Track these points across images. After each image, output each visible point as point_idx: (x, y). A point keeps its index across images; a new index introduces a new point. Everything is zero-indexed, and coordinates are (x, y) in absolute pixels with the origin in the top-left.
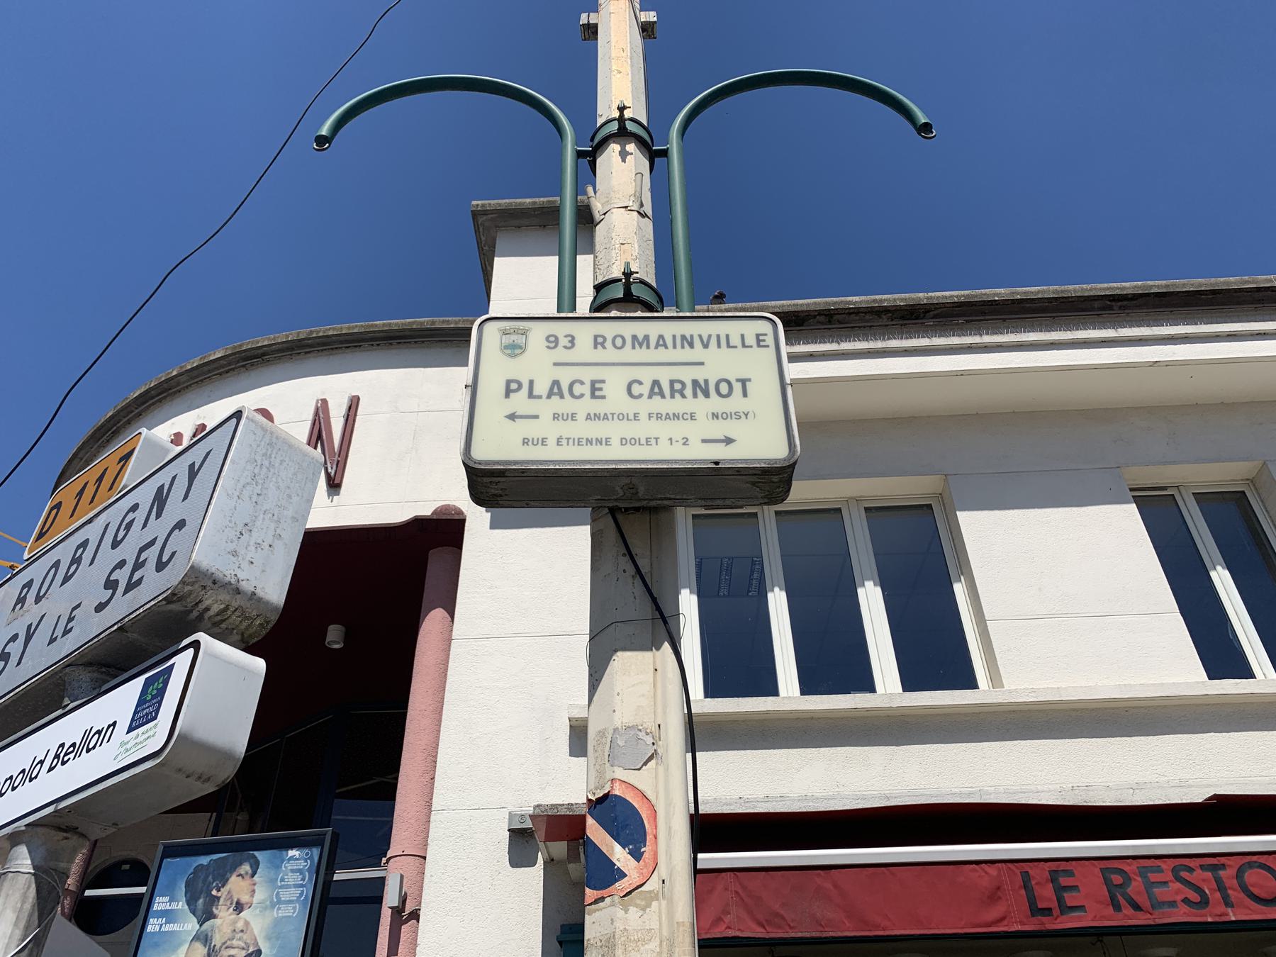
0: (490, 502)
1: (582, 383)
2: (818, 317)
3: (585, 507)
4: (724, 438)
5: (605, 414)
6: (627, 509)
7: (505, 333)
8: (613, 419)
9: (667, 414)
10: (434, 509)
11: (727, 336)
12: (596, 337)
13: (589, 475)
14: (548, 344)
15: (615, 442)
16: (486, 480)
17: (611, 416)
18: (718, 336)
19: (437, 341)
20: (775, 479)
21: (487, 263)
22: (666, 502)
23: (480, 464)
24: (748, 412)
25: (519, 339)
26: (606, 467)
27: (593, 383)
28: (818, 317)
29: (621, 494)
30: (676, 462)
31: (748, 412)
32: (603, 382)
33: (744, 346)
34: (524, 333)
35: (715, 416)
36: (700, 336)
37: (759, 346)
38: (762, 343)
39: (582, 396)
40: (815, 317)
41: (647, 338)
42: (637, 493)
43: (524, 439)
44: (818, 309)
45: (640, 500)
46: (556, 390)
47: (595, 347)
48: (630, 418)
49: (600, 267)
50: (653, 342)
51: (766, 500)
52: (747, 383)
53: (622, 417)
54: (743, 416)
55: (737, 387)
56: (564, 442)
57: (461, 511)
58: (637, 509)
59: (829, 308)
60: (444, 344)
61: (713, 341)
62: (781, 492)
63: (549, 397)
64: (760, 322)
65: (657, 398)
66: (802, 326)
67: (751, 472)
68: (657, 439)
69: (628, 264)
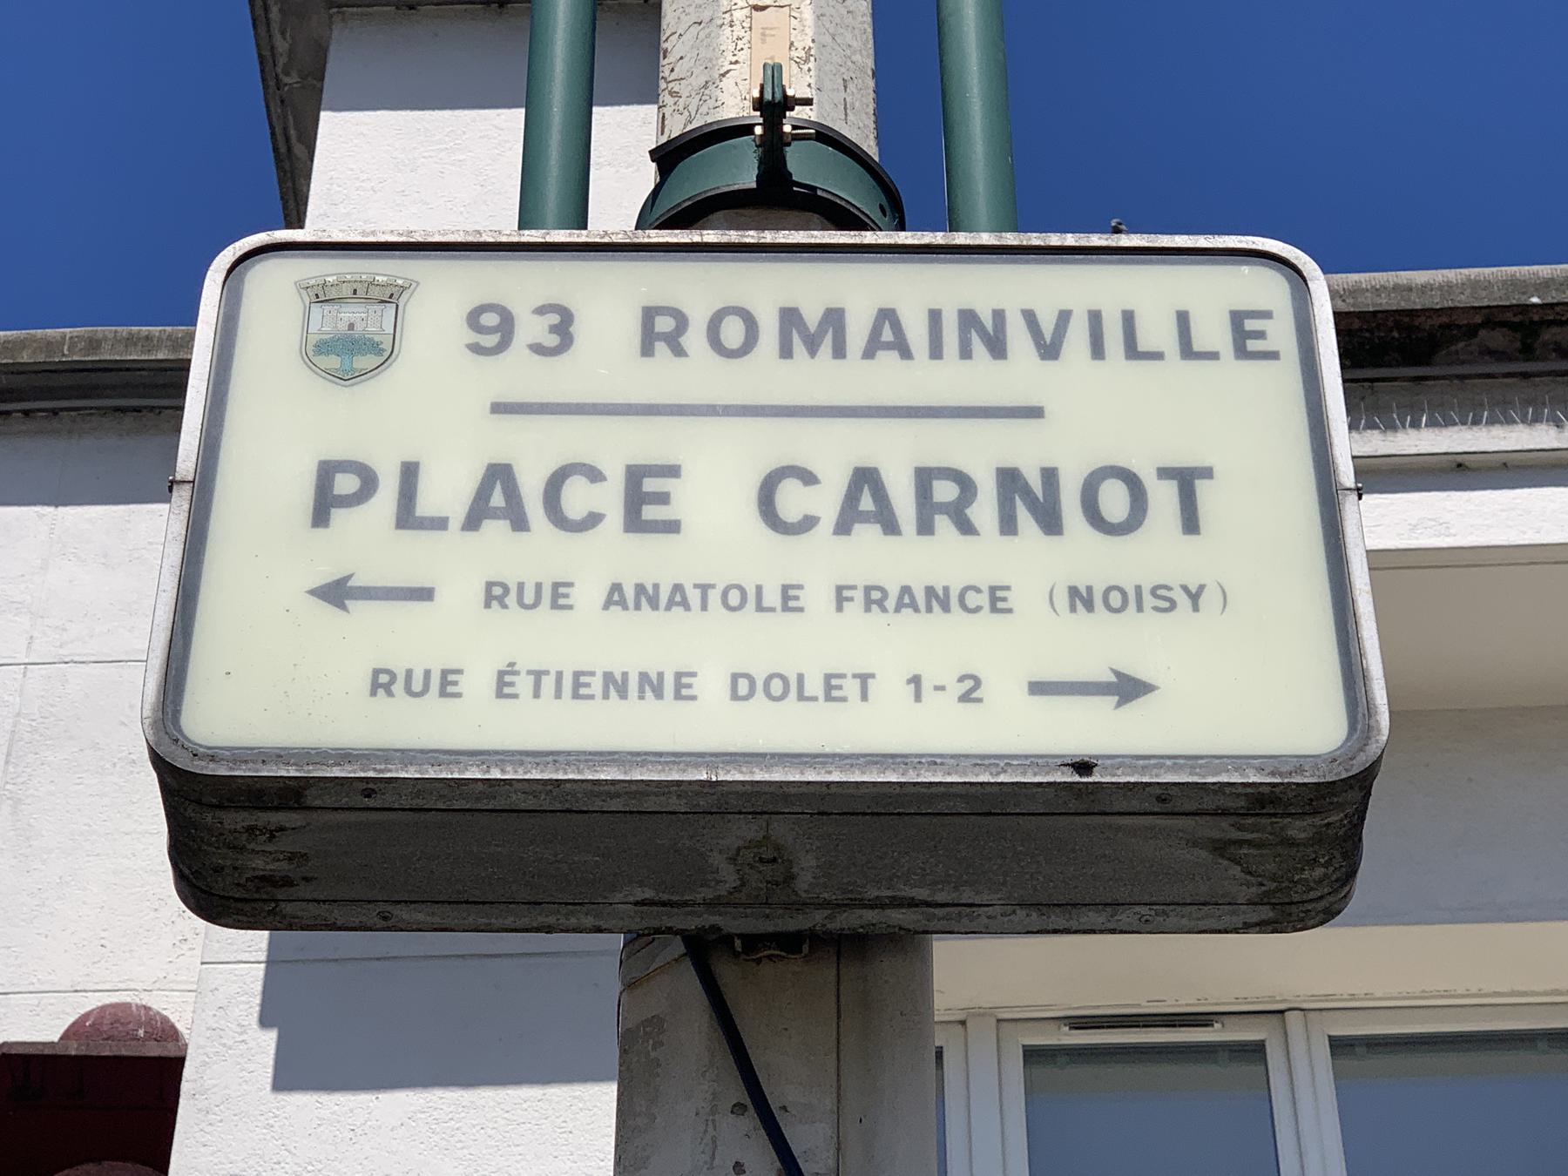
0: (247, 907)
1: (594, 475)
2: (1483, 333)
3: (599, 930)
4: (1113, 679)
5: (678, 588)
6: (753, 942)
7: (321, 296)
8: (704, 607)
9: (906, 590)
10: (71, 1020)
11: (1128, 318)
12: (649, 314)
13: (615, 805)
14: (474, 337)
15: (711, 685)
16: (236, 820)
17: (698, 592)
18: (1095, 318)
19: (104, 411)
20: (1299, 829)
21: (292, 132)
22: (898, 917)
23: (213, 758)
24: (1202, 588)
25: (371, 321)
26: (675, 777)
27: (635, 475)
28: (1483, 333)
29: (730, 877)
30: (934, 761)
31: (1202, 588)
32: (673, 471)
33: (1188, 351)
34: (392, 297)
35: (1081, 598)
36: (1030, 317)
37: (1242, 352)
38: (1252, 345)
39: (593, 520)
40: (1472, 331)
41: (834, 319)
42: (790, 878)
43: (377, 673)
44: (1485, 303)
45: (801, 906)
46: (497, 499)
47: (647, 350)
48: (766, 603)
49: (675, 87)
50: (857, 332)
51: (1266, 913)
52: (1201, 486)
53: (739, 598)
54: (1183, 601)
55: (1163, 497)
56: (524, 684)
57: (173, 1027)
58: (790, 943)
59: (1523, 300)
60: (128, 420)
61: (1078, 337)
62: (1320, 881)
63: (472, 522)
64: (1248, 272)
65: (867, 534)
66: (1428, 364)
67: (1209, 803)
68: (864, 679)
69: (774, 72)
